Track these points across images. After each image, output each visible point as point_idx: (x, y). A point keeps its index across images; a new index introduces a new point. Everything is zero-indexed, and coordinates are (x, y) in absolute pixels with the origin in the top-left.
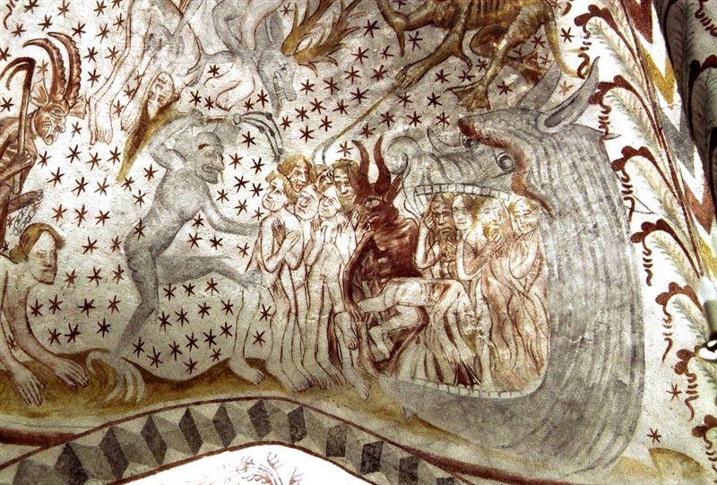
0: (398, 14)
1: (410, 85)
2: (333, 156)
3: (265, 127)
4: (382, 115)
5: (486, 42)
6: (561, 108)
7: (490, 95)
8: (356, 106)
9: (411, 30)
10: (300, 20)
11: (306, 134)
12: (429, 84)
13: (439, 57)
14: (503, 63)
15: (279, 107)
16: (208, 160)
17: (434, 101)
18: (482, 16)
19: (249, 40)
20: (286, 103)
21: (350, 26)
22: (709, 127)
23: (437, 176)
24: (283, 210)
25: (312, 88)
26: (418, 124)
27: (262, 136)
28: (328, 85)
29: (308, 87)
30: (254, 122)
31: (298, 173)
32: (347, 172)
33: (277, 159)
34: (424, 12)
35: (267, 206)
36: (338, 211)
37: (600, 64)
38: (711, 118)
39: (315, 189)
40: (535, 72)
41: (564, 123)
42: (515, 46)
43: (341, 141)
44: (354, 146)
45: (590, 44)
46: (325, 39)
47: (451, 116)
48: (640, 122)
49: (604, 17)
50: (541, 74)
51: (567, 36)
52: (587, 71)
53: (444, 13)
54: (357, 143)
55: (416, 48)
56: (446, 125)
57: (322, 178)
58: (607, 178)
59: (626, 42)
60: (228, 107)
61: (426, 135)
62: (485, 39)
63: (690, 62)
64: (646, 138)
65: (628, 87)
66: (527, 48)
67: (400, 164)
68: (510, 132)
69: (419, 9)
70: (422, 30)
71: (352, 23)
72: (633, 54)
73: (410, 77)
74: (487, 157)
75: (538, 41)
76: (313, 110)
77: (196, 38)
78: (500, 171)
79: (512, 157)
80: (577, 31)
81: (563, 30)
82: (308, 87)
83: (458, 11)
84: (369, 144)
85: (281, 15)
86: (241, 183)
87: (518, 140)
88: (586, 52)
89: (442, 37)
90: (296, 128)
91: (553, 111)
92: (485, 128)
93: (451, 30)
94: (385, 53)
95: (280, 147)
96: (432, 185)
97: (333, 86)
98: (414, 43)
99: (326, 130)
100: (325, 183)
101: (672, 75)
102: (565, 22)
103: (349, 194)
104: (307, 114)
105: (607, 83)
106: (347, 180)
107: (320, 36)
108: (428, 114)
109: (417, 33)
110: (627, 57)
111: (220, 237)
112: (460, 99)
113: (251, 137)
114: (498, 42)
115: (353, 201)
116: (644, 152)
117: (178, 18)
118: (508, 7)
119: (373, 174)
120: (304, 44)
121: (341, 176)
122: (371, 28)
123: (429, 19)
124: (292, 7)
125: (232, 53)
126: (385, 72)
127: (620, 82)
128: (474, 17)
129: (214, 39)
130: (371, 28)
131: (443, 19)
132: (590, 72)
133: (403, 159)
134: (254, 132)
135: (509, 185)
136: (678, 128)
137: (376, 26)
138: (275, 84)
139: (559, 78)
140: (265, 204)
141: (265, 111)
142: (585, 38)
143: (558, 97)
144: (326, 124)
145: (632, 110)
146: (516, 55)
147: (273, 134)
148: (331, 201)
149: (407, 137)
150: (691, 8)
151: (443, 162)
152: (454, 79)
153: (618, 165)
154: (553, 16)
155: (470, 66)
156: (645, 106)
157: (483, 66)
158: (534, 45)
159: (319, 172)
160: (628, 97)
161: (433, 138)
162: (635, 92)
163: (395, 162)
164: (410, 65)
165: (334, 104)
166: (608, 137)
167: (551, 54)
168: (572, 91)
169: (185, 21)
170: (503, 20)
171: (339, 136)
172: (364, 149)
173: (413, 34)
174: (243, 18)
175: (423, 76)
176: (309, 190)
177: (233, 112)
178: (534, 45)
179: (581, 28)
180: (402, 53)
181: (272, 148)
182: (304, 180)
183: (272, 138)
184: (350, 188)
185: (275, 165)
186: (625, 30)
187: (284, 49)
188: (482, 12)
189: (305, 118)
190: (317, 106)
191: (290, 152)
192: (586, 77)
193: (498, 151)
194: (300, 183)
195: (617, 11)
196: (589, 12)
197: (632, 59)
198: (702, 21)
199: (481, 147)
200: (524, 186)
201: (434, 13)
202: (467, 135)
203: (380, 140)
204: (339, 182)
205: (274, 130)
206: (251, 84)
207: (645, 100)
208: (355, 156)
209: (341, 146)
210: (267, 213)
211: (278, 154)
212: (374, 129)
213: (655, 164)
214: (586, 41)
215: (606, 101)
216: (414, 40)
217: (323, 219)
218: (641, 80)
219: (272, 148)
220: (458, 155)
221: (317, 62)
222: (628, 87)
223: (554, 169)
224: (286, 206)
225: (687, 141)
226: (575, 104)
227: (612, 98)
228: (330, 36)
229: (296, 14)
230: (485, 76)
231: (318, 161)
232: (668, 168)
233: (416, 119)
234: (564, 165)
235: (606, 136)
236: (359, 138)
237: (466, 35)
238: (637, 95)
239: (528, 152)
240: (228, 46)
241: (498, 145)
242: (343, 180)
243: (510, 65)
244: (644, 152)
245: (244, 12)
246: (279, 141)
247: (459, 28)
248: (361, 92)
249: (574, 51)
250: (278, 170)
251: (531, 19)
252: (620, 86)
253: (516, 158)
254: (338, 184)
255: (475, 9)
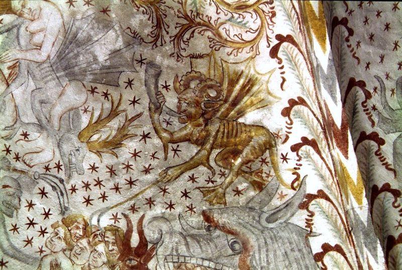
0: (166, 130)
1: (169, 181)
2: (106, 221)
3: (57, 188)
4: (146, 199)
5: (226, 159)
6: (278, 210)
7: (227, 195)
8: (127, 189)
9: (173, 143)
10: (94, 120)
11: (88, 201)
12: (183, 183)
13: (192, 164)
14: (238, 174)
15: (70, 177)
16: (9, 198)
17: (185, 194)
18: (225, 140)
19: (56, 122)
20: (75, 175)
21: (130, 133)
22: (386, 235)
23: (183, 249)
24: (61, 253)
25: (97, 170)
26: (172, 209)
27: (54, 193)
28: (108, 170)
29: (93, 168)
30: (49, 181)
31: (78, 228)
32: (115, 235)
33: (63, 213)
34: (184, 132)
35: (49, 246)
36: (104, 264)
37: (307, 180)
38: (387, 229)
39: (89, 243)
40: (261, 183)
41: (280, 221)
42: (247, 163)
43: (114, 211)
44: (123, 217)
45: (301, 165)
46: (110, 138)
47: (198, 207)
48: (335, 225)
49: (312, 146)
50: (265, 184)
51: (285, 158)
52: (298, 184)
53: (198, 135)
54: (126, 216)
55: (176, 156)
56: (193, 213)
57: (95, 235)
58: (310, 266)
59: (327, 165)
60: (32, 164)
61: (178, 219)
62: (226, 156)
63: (371, 186)
64: (340, 237)
65: (328, 199)
66: (256, 165)
67: (156, 237)
68: (240, 224)
69: (181, 130)
70: (181, 144)
71: (131, 130)
72: (331, 174)
73: (169, 175)
74: (222, 240)
75: (263, 161)
76: (95, 185)
77: (16, 106)
78: (230, 252)
79: (239, 241)
80: (292, 156)
81: (282, 154)
82: (93, 168)
83: (208, 135)
84: (135, 218)
85: (81, 112)
86: (31, 224)
87: (245, 230)
88: (297, 171)
89: (196, 151)
90: (81, 194)
91: (272, 212)
92: (221, 218)
93: (202, 147)
94: (153, 156)
95: (66, 205)
96: (178, 256)
97: (112, 172)
98: (175, 153)
99: (103, 201)
100: (97, 240)
101: (361, 184)
102: (284, 148)
103: (114, 252)
104: (90, 187)
105: (312, 195)
106: (114, 241)
107: (108, 135)
108: (181, 204)
109: (178, 146)
110: (327, 177)
111: (7, 260)
112: (204, 196)
113: (45, 192)
114: (235, 160)
115: (117, 258)
116: (338, 249)
117: (5, 86)
118: (244, 136)
119: (135, 241)
120: (95, 137)
121: (110, 237)
122: (145, 136)
123: (187, 138)
124: (90, 109)
125: (41, 127)
126: (152, 169)
127: (321, 194)
128: (219, 140)
129: (30, 112)
130: (145, 136)
131: (197, 139)
132: (300, 186)
133: (159, 233)
134: (48, 189)
135: (237, 264)
136: (366, 224)
137: (149, 136)
138: (69, 159)
139: (278, 189)
140: (48, 244)
141: (58, 176)
142: (298, 160)
143: (276, 202)
144: (104, 197)
145: (330, 216)
146: (248, 170)
147: (62, 194)
148: (100, 255)
149: (163, 218)
150: (372, 148)
151: (189, 240)
152: (201, 181)
153: (319, 257)
154: (276, 144)
155: (214, 174)
156: (339, 214)
157: (223, 175)
158: (261, 163)
159: (93, 230)
160: (328, 205)
161: (182, 221)
162: (332, 202)
163: (152, 235)
164: (171, 167)
165: (111, 184)
166: (312, 234)
167: (272, 171)
168: (287, 198)
169: (10, 90)
170: (240, 144)
171: (112, 208)
172: (131, 222)
173: (175, 146)
174: (54, 106)
175: (179, 176)
176: (84, 242)
177: (34, 169)
178: (261, 163)
179: (295, 153)
180: (166, 159)
181: (60, 204)
182: (81, 233)
183: (61, 197)
184: (115, 248)
185: (60, 218)
186: (327, 157)
187: (80, 136)
188: (225, 137)
189: (88, 189)
190: (99, 183)
191: (73, 211)
192: (297, 189)
193: (230, 237)
194: (77, 235)
195: (322, 141)
196: (301, 142)
197: (331, 178)
198: (380, 158)
199: (218, 232)
200: (248, 266)
201: (191, 134)
202: (208, 222)
203: (143, 217)
204: (108, 241)
205: (64, 192)
206: (51, 153)
207: (339, 209)
208: (122, 224)
209: (113, 215)
210: (48, 252)
211: (64, 210)
212: (139, 208)
213: (346, 258)
214: (299, 163)
215: (311, 208)
216: (175, 151)
217: (92, 267)
218: (336, 194)
219: (60, 204)
220: (201, 236)
221: (103, 152)
222: (328, 199)
223: (271, 256)
224: (64, 250)
225: (372, 235)
226: (289, 207)
227: (316, 206)
228: (115, 137)
229: (92, 115)
230: (224, 182)
231: (94, 222)
232: (356, 262)
233: (171, 206)
234: (278, 253)
235: (310, 233)
236: (127, 212)
237: (213, 152)
238: (334, 205)
239: (253, 241)
240: (39, 121)
241: (230, 232)
242: (111, 241)
243: (243, 176)
244: (338, 249)
245: (55, 101)
246: (66, 200)
247: (208, 146)
248: (132, 180)
249: (289, 170)
250: (62, 221)
251: (260, 145)
252: (322, 198)
253: (243, 244)
254: (107, 243)
255: (220, 135)
